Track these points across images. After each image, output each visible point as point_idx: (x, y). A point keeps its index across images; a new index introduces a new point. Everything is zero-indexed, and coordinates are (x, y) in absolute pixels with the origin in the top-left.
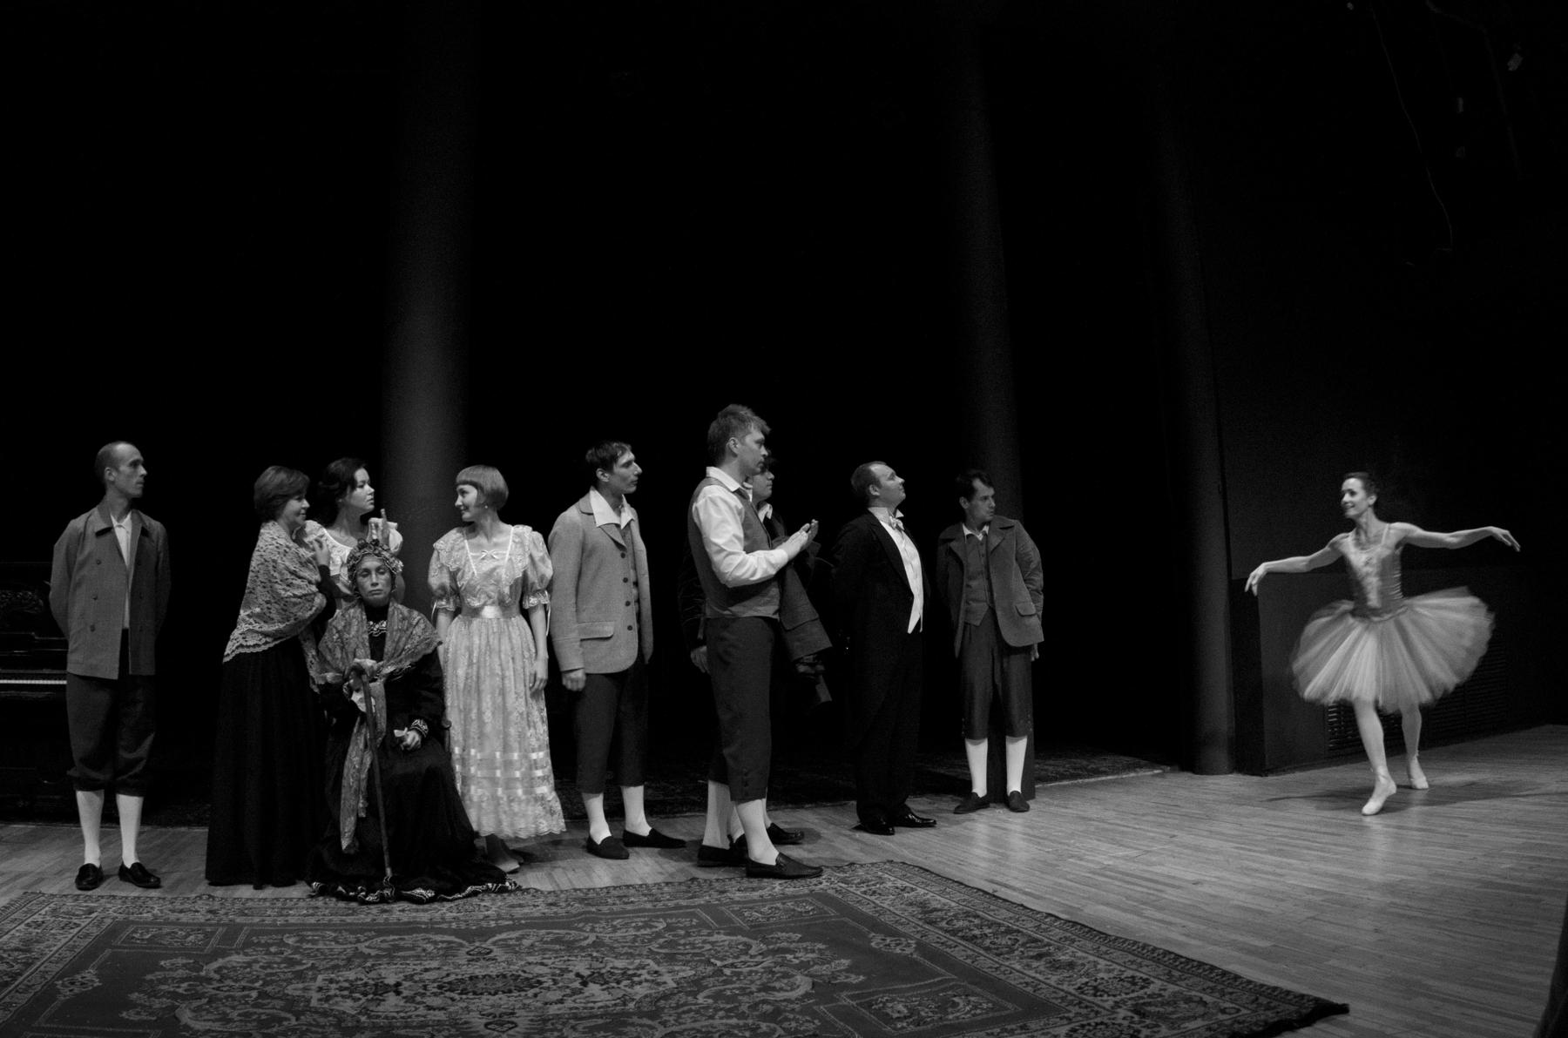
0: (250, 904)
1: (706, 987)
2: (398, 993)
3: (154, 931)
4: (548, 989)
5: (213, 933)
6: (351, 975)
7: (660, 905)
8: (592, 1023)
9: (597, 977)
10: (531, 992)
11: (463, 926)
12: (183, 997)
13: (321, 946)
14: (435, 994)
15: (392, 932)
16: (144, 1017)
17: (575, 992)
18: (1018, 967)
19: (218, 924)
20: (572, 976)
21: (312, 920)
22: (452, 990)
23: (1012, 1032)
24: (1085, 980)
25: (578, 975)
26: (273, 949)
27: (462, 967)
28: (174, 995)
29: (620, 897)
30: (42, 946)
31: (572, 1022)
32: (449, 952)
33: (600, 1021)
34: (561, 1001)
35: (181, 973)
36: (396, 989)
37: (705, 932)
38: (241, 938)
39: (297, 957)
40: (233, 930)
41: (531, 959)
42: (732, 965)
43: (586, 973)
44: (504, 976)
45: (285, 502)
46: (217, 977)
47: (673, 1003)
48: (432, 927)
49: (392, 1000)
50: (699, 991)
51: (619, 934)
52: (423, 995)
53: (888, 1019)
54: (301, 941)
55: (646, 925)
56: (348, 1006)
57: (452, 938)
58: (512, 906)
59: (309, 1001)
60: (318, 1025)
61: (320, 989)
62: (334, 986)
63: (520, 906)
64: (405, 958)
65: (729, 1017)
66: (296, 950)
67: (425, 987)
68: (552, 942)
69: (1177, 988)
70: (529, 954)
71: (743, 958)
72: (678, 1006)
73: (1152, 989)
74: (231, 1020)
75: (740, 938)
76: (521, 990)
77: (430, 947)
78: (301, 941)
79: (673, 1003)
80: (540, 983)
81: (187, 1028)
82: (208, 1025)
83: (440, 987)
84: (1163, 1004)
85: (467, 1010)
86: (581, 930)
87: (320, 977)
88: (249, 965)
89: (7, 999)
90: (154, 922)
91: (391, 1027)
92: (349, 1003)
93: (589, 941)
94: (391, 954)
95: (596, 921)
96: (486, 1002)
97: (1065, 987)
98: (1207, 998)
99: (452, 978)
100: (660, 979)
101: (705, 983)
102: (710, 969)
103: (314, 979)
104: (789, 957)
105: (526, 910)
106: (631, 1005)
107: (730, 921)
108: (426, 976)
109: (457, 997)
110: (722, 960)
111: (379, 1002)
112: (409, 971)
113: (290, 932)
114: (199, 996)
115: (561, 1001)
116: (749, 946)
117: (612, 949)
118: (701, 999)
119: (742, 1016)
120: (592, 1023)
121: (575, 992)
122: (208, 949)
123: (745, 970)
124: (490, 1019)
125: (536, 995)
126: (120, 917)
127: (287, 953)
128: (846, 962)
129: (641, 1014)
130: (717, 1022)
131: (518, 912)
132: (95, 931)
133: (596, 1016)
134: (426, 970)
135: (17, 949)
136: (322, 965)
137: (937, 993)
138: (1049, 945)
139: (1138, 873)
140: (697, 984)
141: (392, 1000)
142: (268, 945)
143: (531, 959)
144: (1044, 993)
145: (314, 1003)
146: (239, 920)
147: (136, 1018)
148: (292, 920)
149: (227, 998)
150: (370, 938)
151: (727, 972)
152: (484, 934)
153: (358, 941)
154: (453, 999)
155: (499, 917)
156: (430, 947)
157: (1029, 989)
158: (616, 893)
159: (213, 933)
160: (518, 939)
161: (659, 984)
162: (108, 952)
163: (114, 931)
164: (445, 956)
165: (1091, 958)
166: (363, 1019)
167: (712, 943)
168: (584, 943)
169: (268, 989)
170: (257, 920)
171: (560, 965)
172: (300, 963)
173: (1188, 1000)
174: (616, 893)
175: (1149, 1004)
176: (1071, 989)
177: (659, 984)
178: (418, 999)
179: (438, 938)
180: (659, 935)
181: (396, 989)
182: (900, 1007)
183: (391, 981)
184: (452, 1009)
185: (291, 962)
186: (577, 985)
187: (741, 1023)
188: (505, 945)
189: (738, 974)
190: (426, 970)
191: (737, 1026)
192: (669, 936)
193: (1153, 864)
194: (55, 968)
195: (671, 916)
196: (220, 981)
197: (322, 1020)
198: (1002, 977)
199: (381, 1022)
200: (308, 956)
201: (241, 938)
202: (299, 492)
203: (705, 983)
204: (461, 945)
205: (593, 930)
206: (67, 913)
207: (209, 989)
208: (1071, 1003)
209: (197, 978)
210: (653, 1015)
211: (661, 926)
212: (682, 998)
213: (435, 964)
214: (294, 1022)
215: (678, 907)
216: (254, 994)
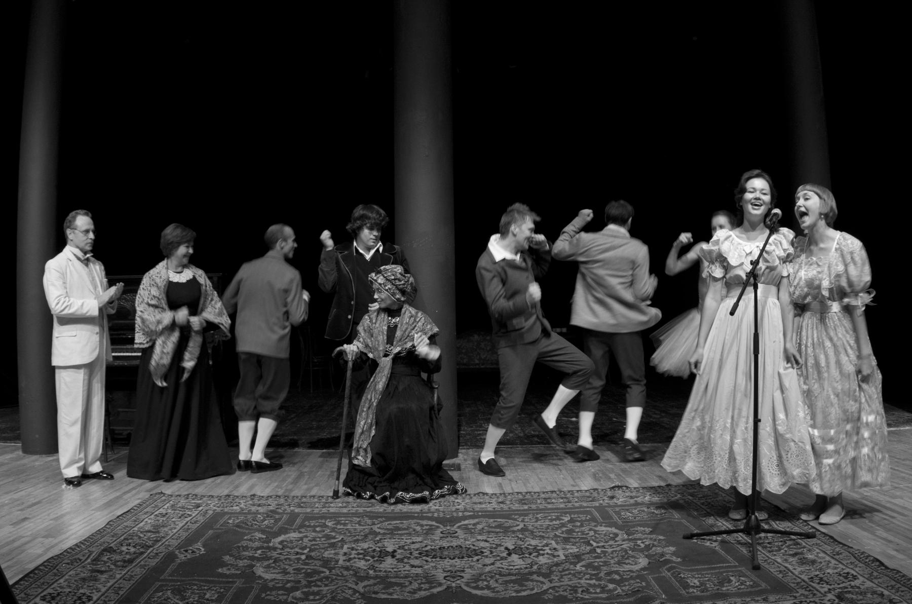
0: (304, 500)
1: (584, 560)
2: (393, 557)
3: (242, 518)
4: (487, 557)
5: (280, 519)
6: (365, 545)
7: (570, 505)
8: (508, 578)
9: (518, 550)
10: (476, 558)
11: (441, 515)
12: (258, 559)
13: (349, 527)
14: (416, 558)
15: (395, 519)
16: (233, 571)
17: (502, 558)
18: (779, 560)
19: (283, 513)
20: (502, 549)
21: (345, 511)
22: (427, 556)
23: (758, 601)
24: (818, 573)
25: (506, 548)
26: (318, 529)
27: (437, 540)
28: (252, 558)
29: (545, 499)
30: (166, 529)
31: (497, 576)
32: (430, 531)
33: (514, 578)
34: (493, 564)
35: (257, 544)
36: (393, 554)
37: (594, 524)
38: (298, 521)
39: (333, 534)
40: (293, 516)
41: (480, 537)
42: (603, 547)
43: (511, 547)
44: (441, 558)
45: (179, 246)
46: (280, 547)
47: (560, 568)
48: (421, 516)
49: (389, 560)
50: (578, 562)
51: (539, 523)
52: (409, 558)
53: (686, 586)
54: (336, 524)
55: (558, 518)
56: (362, 564)
57: (434, 523)
58: (475, 503)
59: (337, 561)
60: (343, 576)
61: (345, 554)
62: (354, 552)
63: (480, 503)
64: (401, 535)
65: (591, 579)
66: (333, 530)
67: (411, 553)
68: (496, 527)
69: (872, 584)
70: (480, 534)
71: (611, 543)
72: (564, 570)
73: (856, 583)
74: (289, 573)
75: (614, 530)
76: (470, 556)
77: (418, 528)
78: (336, 524)
79: (560, 568)
80: (482, 552)
81: (260, 577)
82: (274, 576)
83: (420, 554)
84: (857, 593)
85: (435, 568)
86: (515, 520)
87: (346, 547)
88: (301, 539)
89: (142, 563)
90: (241, 512)
91: (387, 577)
92: (363, 562)
93: (519, 528)
94: (392, 532)
95: (526, 515)
96: (447, 563)
97: (802, 577)
98: (886, 593)
99: (428, 548)
100: (556, 553)
101: (583, 557)
102: (588, 548)
103: (342, 547)
104: (639, 542)
105: (483, 506)
106: (535, 567)
107: (611, 518)
108: (412, 546)
109: (430, 560)
110: (597, 543)
111: (381, 562)
112: (402, 543)
113: (330, 518)
114: (268, 559)
115: (493, 564)
116: (616, 535)
117: (532, 532)
118: (578, 567)
119: (599, 579)
120: (508, 578)
121: (502, 558)
122: (275, 529)
123: (610, 550)
124: (449, 574)
125: (478, 560)
126: (218, 510)
127: (327, 531)
128: (672, 549)
129: (539, 573)
130: (582, 581)
131: (478, 507)
132: (201, 519)
133: (512, 575)
134: (413, 543)
135: (149, 531)
136: (348, 539)
137: (722, 573)
138: (804, 547)
139: (883, 503)
140: (578, 557)
141: (389, 560)
142: (315, 526)
143: (480, 537)
144: (788, 579)
145: (341, 562)
146: (296, 511)
147: (228, 572)
148: (332, 510)
149: (286, 559)
150: (381, 522)
151: (599, 550)
152: (453, 521)
153: (374, 524)
154: (427, 561)
155: (465, 510)
156: (418, 528)
157: (780, 576)
158: (543, 496)
159: (280, 519)
160: (474, 525)
161: (554, 556)
162: (211, 532)
163: (217, 516)
164: (427, 534)
165: (828, 558)
166: (371, 572)
167: (595, 531)
168: (516, 529)
169: (313, 554)
170: (309, 510)
171: (497, 542)
172: (334, 538)
173: (874, 593)
174: (543, 496)
175: (849, 592)
176: (806, 579)
177: (554, 556)
178: (406, 560)
179: (425, 522)
180: (563, 525)
181: (393, 554)
182: (696, 581)
183: (390, 549)
184: (426, 567)
185: (328, 537)
186: (505, 555)
187: (597, 583)
188: (466, 528)
189: (604, 553)
190: (413, 543)
191: (594, 586)
192: (570, 526)
193: (896, 497)
194: (175, 543)
195: (574, 513)
196: (282, 549)
197: (345, 573)
198: (767, 566)
199: (382, 574)
200: (340, 533)
201: (298, 521)
202: (188, 242)
203: (583, 557)
204: (438, 527)
205: (523, 521)
206: (183, 507)
207: (275, 554)
208: (802, 587)
209: (269, 548)
210: (545, 576)
211: (566, 519)
212: (567, 566)
213: (420, 539)
214: (328, 573)
215: (581, 507)
216: (303, 557)
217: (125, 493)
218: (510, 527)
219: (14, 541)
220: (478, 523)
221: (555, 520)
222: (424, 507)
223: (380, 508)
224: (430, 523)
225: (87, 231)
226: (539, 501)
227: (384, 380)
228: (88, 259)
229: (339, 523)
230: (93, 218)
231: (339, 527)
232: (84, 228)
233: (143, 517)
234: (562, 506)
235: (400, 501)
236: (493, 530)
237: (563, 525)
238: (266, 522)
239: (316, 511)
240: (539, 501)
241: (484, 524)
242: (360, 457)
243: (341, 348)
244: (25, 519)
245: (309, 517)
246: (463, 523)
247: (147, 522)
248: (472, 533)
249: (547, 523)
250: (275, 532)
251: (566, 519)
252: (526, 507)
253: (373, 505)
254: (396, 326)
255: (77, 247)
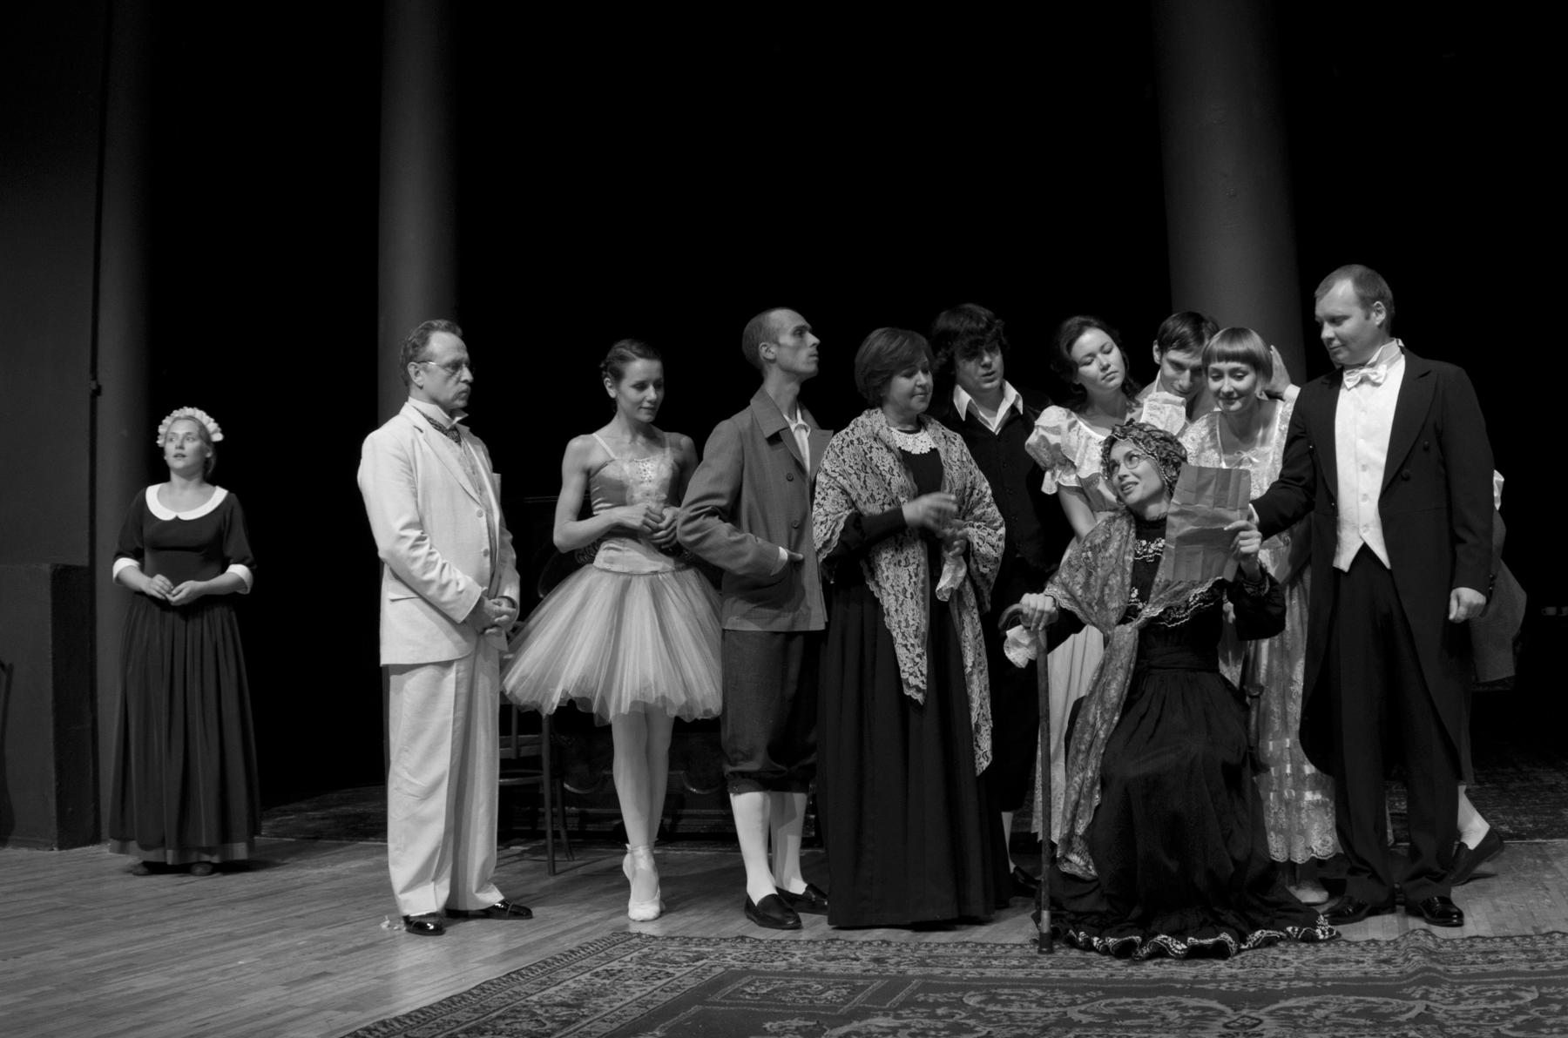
7: (1541, 967)
11: (1237, 987)
13: (1015, 1009)
26: (940, 1011)
29: (1485, 953)
30: (600, 1001)
39: (972, 1022)
40: (901, 981)
51: (1462, 1007)
54: (986, 1002)
55: (1509, 995)
63: (1336, 961)
66: (975, 1013)
68: (1358, 1014)
77: (1174, 1015)
78: (986, 1002)
90: (787, 974)
105: (1342, 968)
113: (977, 989)
127: (960, 1016)
131: (1329, 970)
132: (691, 983)
142: (938, 1005)
148: (989, 973)
150: (1092, 1000)
152: (1263, 997)
153: (1073, 1003)
155: (1298, 976)
156: (1174, 1015)
158: (1481, 946)
160: (1309, 1008)
170: (938, 971)
174: (1481, 946)
180: (1520, 1010)
192: (1534, 1013)
195: (1549, 983)
205: (1425, 997)
217: (564, 933)
218: (1394, 1014)
219: (269, 1014)
220: (1318, 1006)
221: (1502, 998)
222: (1222, 967)
223: (1120, 969)
224: (1206, 1003)
225: (455, 366)
226: (1469, 958)
227: (1120, 677)
228: (454, 429)
229: (993, 999)
230: (464, 338)
231: (991, 1007)
232: (448, 358)
233: (566, 976)
234: (1524, 967)
235: (1161, 953)
236: (1350, 1020)
237: (1520, 1010)
238: (829, 994)
239: (955, 973)
240: (1469, 958)
241: (1333, 1008)
242: (1075, 858)
243: (1015, 607)
244: (325, 974)
245: (928, 985)
246: (1283, 1004)
247: (571, 983)
248: (1297, 1026)
249: (1483, 1004)
250: (841, 1016)
251: (1529, 997)
252: (1440, 968)
253: (1089, 963)
254: (1157, 559)
255: (435, 401)
